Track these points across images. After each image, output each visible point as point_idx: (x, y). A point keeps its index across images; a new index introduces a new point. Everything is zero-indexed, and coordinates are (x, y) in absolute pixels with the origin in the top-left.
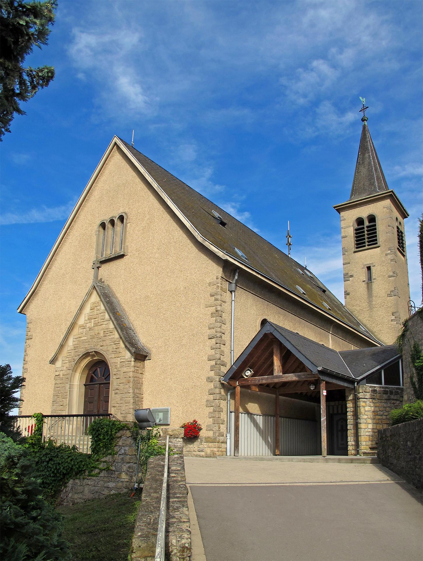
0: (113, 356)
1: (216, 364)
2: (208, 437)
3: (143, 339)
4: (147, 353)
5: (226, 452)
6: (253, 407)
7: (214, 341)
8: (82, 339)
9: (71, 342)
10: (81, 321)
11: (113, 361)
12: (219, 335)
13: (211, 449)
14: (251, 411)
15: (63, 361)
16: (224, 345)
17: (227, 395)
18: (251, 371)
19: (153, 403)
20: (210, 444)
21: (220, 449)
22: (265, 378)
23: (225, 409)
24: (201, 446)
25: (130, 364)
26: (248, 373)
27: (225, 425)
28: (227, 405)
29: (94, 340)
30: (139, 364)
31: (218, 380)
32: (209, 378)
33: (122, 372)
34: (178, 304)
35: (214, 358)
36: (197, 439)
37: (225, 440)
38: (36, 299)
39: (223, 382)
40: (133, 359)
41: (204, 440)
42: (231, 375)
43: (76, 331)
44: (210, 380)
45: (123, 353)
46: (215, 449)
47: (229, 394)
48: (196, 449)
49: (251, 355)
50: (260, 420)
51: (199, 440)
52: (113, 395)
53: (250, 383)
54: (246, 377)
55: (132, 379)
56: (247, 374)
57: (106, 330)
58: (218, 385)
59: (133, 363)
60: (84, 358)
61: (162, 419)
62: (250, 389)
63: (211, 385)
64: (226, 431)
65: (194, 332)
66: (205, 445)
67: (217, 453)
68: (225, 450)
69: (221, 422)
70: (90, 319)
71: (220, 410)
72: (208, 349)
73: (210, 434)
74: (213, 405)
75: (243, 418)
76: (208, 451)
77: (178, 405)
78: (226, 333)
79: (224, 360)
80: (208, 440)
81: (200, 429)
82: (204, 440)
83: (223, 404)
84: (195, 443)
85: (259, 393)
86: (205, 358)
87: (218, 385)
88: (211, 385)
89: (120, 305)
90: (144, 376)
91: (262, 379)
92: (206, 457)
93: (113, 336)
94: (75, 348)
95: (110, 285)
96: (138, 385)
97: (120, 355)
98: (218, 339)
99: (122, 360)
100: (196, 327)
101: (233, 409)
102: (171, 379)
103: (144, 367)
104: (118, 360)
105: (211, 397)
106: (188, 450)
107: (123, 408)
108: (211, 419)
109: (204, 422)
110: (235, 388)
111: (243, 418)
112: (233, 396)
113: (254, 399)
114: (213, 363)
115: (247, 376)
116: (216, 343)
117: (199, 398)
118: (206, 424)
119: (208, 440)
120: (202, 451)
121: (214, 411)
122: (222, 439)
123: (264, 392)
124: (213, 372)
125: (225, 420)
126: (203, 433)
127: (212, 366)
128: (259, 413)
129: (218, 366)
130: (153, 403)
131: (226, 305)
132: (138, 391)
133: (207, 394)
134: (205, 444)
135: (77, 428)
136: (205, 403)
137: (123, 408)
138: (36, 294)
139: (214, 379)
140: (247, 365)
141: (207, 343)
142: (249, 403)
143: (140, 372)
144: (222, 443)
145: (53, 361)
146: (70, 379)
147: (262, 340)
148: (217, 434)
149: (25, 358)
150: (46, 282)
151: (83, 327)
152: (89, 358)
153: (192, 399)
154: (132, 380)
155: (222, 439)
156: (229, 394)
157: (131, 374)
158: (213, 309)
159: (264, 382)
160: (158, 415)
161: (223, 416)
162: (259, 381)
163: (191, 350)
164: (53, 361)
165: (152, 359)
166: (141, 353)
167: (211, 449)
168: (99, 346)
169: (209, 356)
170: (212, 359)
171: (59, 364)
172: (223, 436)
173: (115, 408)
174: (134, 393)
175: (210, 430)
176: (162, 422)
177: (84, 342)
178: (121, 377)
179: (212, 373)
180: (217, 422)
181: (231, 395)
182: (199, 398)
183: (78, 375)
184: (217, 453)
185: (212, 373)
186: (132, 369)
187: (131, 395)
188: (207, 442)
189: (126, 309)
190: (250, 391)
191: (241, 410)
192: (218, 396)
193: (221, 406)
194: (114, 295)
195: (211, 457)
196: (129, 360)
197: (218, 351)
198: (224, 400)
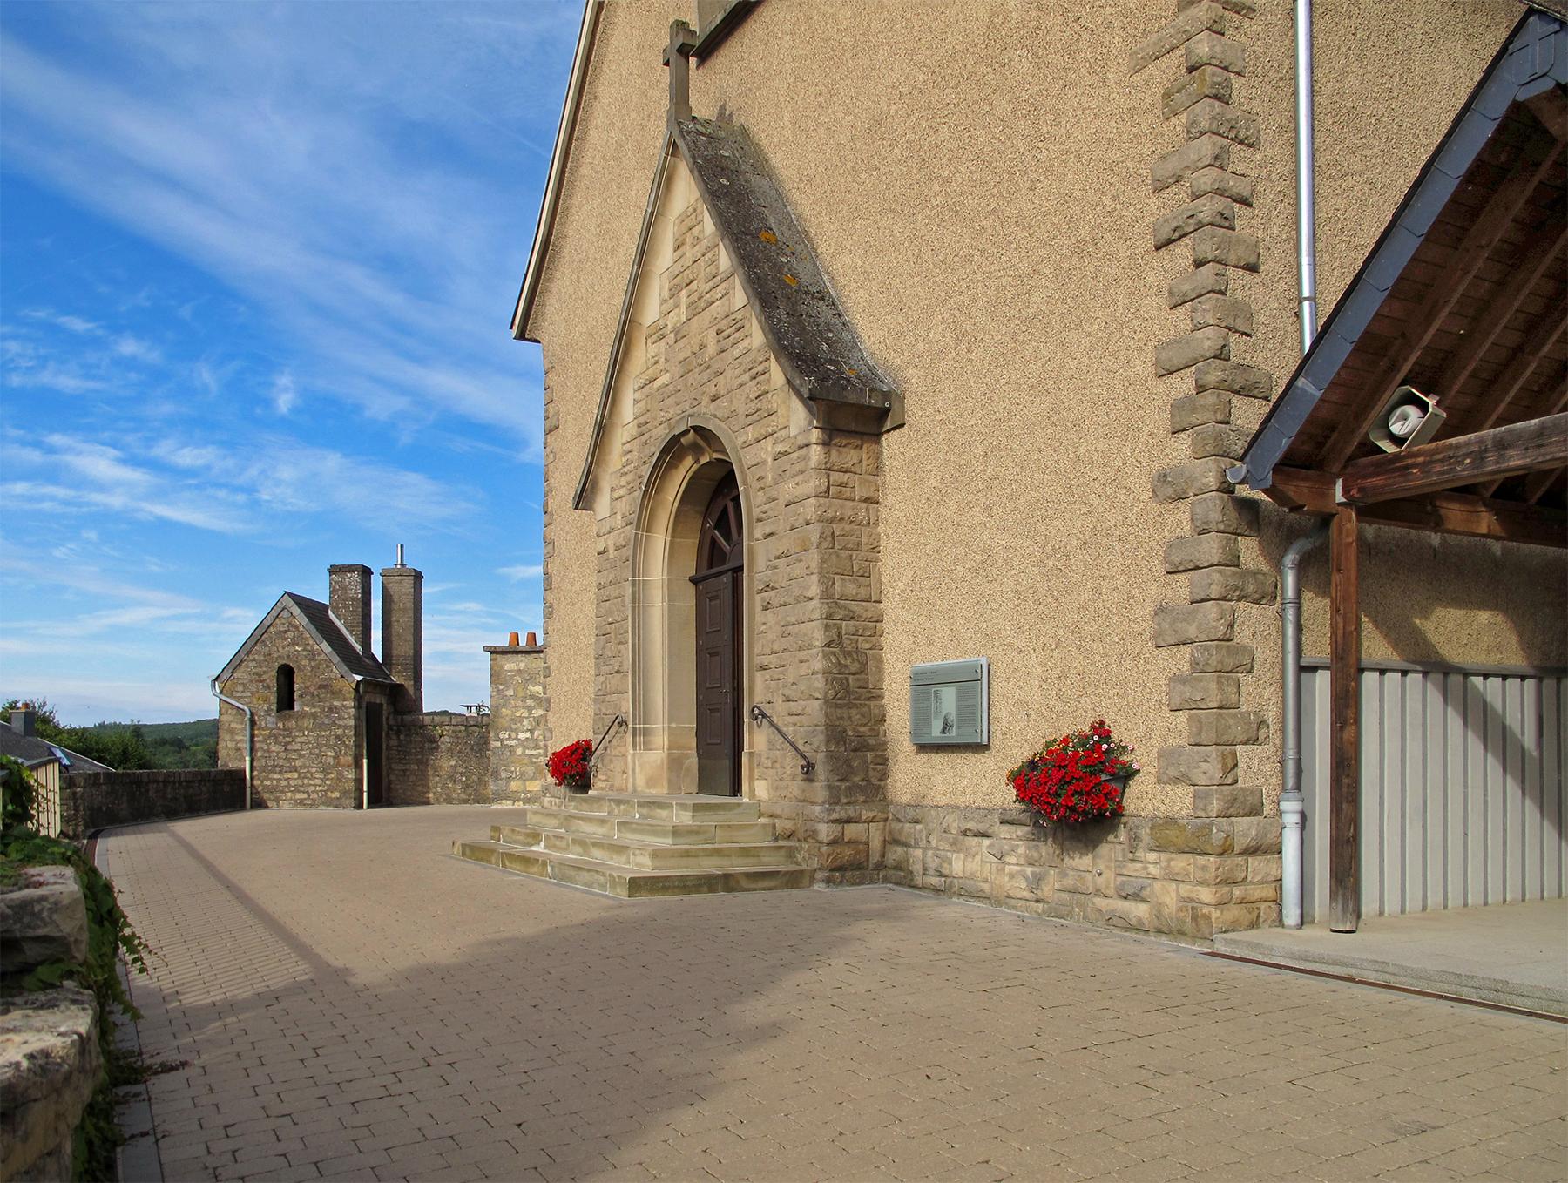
0: (751, 433)
1: (1201, 388)
2: (1170, 821)
3: (879, 333)
4: (887, 395)
5: (1279, 901)
6: (1473, 632)
7: (1182, 252)
8: (657, 383)
9: (628, 409)
10: (651, 312)
11: (754, 459)
12: (1208, 209)
13: (1185, 890)
14: (1452, 653)
15: (613, 490)
16: (1253, 268)
17: (1278, 566)
18: (1424, 407)
19: (922, 640)
20: (1180, 863)
21: (1237, 892)
22: (1519, 435)
23: (1265, 655)
24: (1133, 869)
25: (805, 458)
26: (1407, 421)
27: (1269, 749)
28: (1279, 628)
29: (691, 378)
30: (850, 456)
31: (1212, 481)
32: (1163, 477)
33: (782, 503)
34: (1003, 106)
35: (1188, 354)
36: (1113, 828)
37: (1271, 838)
38: (558, 275)
39: (1243, 491)
40: (815, 435)
41: (1145, 833)
42: (1285, 443)
43: (642, 355)
44: (1169, 487)
45: (782, 411)
46: (1206, 895)
47: (1290, 559)
48: (1109, 880)
49: (1415, 291)
50: (1516, 704)
51: (1123, 834)
52: (760, 616)
53: (1416, 481)
54: (1388, 447)
55: (814, 533)
56: (1396, 428)
57: (723, 325)
58: (1214, 507)
59: (816, 453)
60: (673, 465)
61: (953, 718)
62: (1437, 524)
63: (1181, 519)
64: (1274, 780)
65: (1084, 232)
66: (1154, 863)
67: (1215, 913)
68: (1269, 892)
69: (1238, 732)
70: (674, 292)
71: (1230, 663)
72: (1155, 306)
73: (1180, 801)
74: (1192, 632)
75: (1394, 706)
76: (1169, 897)
77: (1020, 643)
78: (1266, 199)
79: (1257, 359)
80: (1171, 837)
81: (1128, 774)
82: (1145, 833)
83: (1257, 626)
84: (1104, 849)
85: (1496, 547)
86: (1143, 366)
87: (1215, 515)
88: (1181, 519)
89: (781, 198)
90: (884, 513)
91: (1501, 445)
92: (1159, 931)
93: (745, 343)
94: (643, 426)
95: (754, 129)
96: (848, 557)
97: (772, 424)
98: (1214, 236)
99: (780, 448)
100: (1092, 198)
101: (1319, 648)
102: (988, 508)
103: (878, 470)
104: (768, 449)
105: (1181, 588)
106: (1069, 882)
107: (791, 674)
108: (1182, 717)
109: (1148, 733)
110: (1325, 520)
111: (1394, 706)
112: (1315, 567)
113: (1468, 579)
114: (1184, 384)
115: (1398, 440)
116: (1199, 264)
117: (1116, 597)
118: (1156, 744)
119: (1171, 837)
120: (1136, 897)
121: (1198, 669)
122: (1245, 829)
123: (1528, 538)
124: (1185, 439)
125: (1271, 715)
126: (1144, 798)
127: (1178, 407)
128: (1515, 658)
129: (1210, 398)
130: (922, 640)
131: (1253, 27)
132: (851, 589)
133: (1160, 569)
134: (1152, 856)
135: (674, 763)
136: (1148, 626)
137: (791, 674)
138: (555, 253)
139: (1190, 480)
140: (1393, 368)
141: (1151, 279)
142: (1440, 612)
143: (860, 492)
144: (1251, 851)
145: (584, 498)
146: (636, 561)
147: (1486, 176)
148: (1215, 806)
149: (545, 505)
150: (577, 200)
151: (659, 333)
152: (688, 461)
153: (1084, 607)
154: (815, 538)
155: (1245, 829)
156: (1290, 559)
157: (810, 509)
158: (1173, 65)
159: (1516, 460)
160: (938, 698)
161: (1260, 694)
162: (1480, 457)
163: (1073, 336)
164: (584, 498)
165: (909, 420)
166: (852, 398)
167: (1185, 890)
168: (706, 400)
169: (1161, 347)
170: (1178, 361)
171: (603, 504)
172: (1256, 810)
173: (767, 674)
174: (827, 595)
175: (1177, 780)
176: (953, 736)
177: (663, 395)
178: (781, 526)
179: (1182, 448)
180: (1225, 732)
181: (1302, 567)
182: (1116, 597)
183: (659, 542)
184: (1215, 913)
185: (1182, 448)
186: (815, 483)
187: (816, 608)
188: (1160, 848)
189: (807, 212)
190: (1435, 539)
191: (1375, 646)
192: (1215, 581)
193: (1243, 635)
194: (762, 167)
195: (1182, 933)
196: (801, 441)
197: (1207, 310)
198: (1267, 596)
